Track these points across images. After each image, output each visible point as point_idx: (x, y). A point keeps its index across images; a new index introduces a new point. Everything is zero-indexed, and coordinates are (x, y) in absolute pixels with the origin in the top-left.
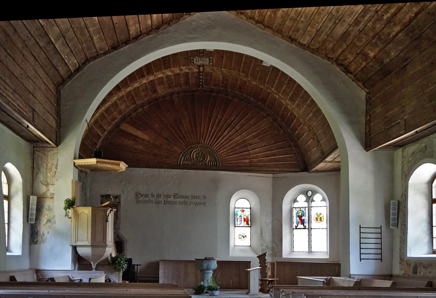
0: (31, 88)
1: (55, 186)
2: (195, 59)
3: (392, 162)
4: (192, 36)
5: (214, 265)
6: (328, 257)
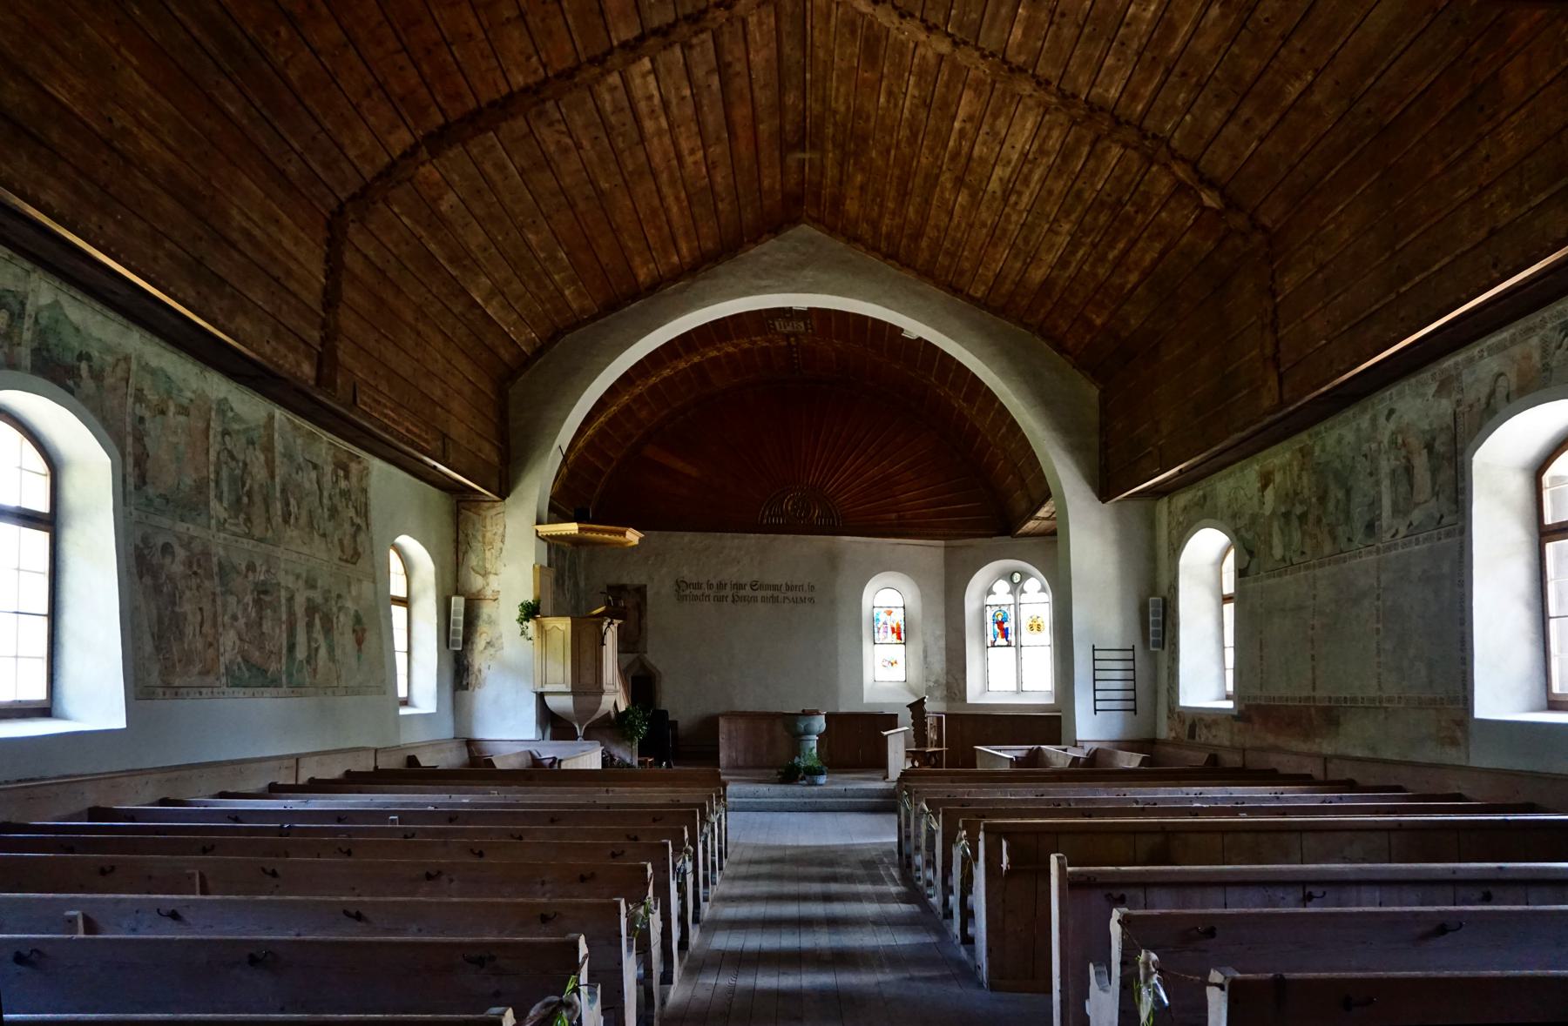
0: (437, 393)
1: (500, 576)
2: (777, 323)
3: (1152, 524)
4: (763, 283)
5: (820, 724)
6: (1053, 702)
